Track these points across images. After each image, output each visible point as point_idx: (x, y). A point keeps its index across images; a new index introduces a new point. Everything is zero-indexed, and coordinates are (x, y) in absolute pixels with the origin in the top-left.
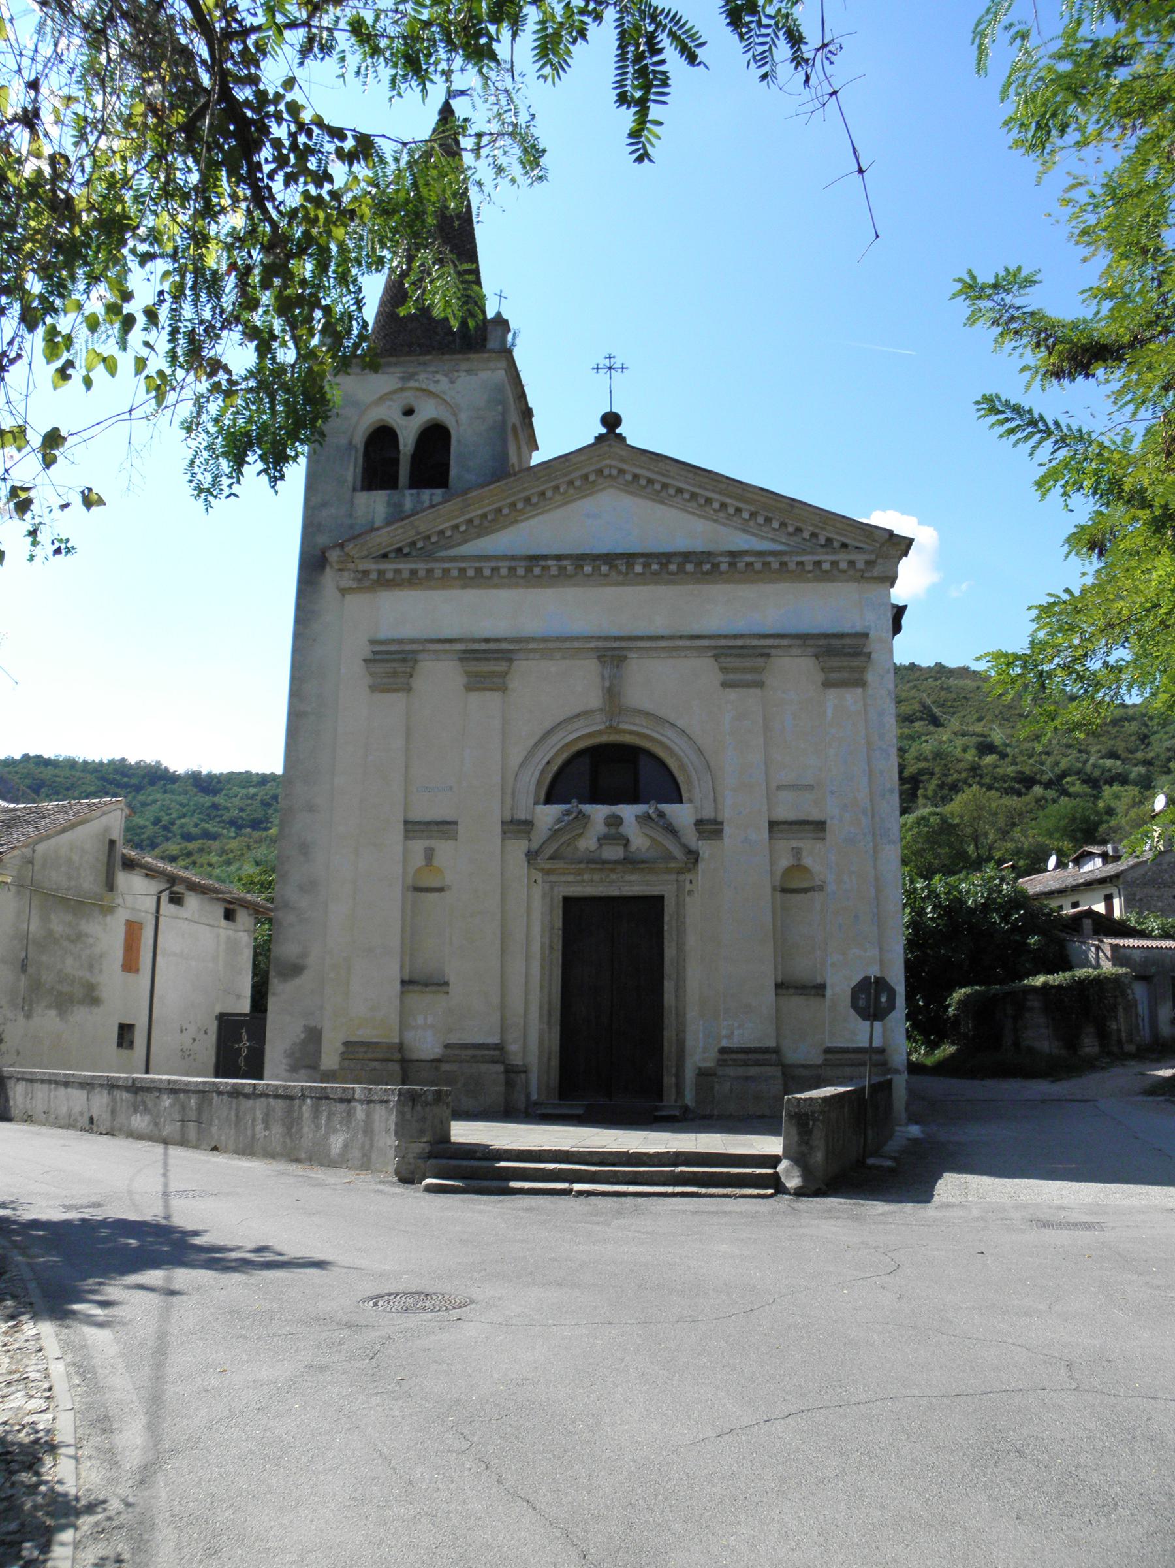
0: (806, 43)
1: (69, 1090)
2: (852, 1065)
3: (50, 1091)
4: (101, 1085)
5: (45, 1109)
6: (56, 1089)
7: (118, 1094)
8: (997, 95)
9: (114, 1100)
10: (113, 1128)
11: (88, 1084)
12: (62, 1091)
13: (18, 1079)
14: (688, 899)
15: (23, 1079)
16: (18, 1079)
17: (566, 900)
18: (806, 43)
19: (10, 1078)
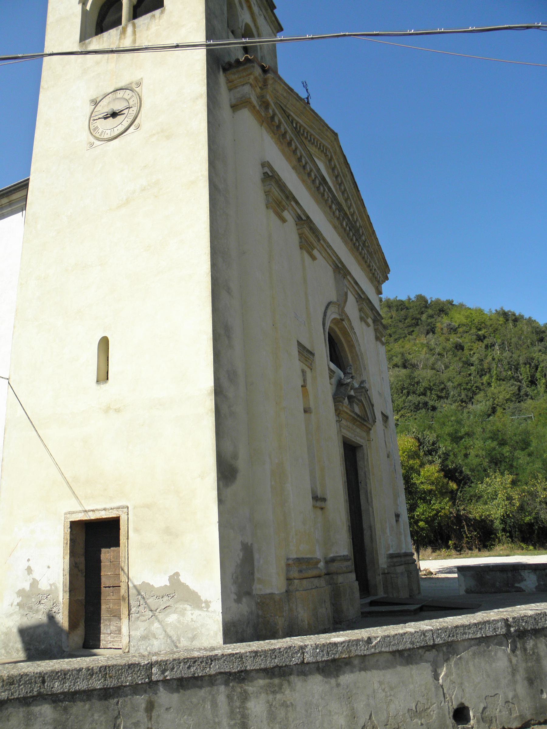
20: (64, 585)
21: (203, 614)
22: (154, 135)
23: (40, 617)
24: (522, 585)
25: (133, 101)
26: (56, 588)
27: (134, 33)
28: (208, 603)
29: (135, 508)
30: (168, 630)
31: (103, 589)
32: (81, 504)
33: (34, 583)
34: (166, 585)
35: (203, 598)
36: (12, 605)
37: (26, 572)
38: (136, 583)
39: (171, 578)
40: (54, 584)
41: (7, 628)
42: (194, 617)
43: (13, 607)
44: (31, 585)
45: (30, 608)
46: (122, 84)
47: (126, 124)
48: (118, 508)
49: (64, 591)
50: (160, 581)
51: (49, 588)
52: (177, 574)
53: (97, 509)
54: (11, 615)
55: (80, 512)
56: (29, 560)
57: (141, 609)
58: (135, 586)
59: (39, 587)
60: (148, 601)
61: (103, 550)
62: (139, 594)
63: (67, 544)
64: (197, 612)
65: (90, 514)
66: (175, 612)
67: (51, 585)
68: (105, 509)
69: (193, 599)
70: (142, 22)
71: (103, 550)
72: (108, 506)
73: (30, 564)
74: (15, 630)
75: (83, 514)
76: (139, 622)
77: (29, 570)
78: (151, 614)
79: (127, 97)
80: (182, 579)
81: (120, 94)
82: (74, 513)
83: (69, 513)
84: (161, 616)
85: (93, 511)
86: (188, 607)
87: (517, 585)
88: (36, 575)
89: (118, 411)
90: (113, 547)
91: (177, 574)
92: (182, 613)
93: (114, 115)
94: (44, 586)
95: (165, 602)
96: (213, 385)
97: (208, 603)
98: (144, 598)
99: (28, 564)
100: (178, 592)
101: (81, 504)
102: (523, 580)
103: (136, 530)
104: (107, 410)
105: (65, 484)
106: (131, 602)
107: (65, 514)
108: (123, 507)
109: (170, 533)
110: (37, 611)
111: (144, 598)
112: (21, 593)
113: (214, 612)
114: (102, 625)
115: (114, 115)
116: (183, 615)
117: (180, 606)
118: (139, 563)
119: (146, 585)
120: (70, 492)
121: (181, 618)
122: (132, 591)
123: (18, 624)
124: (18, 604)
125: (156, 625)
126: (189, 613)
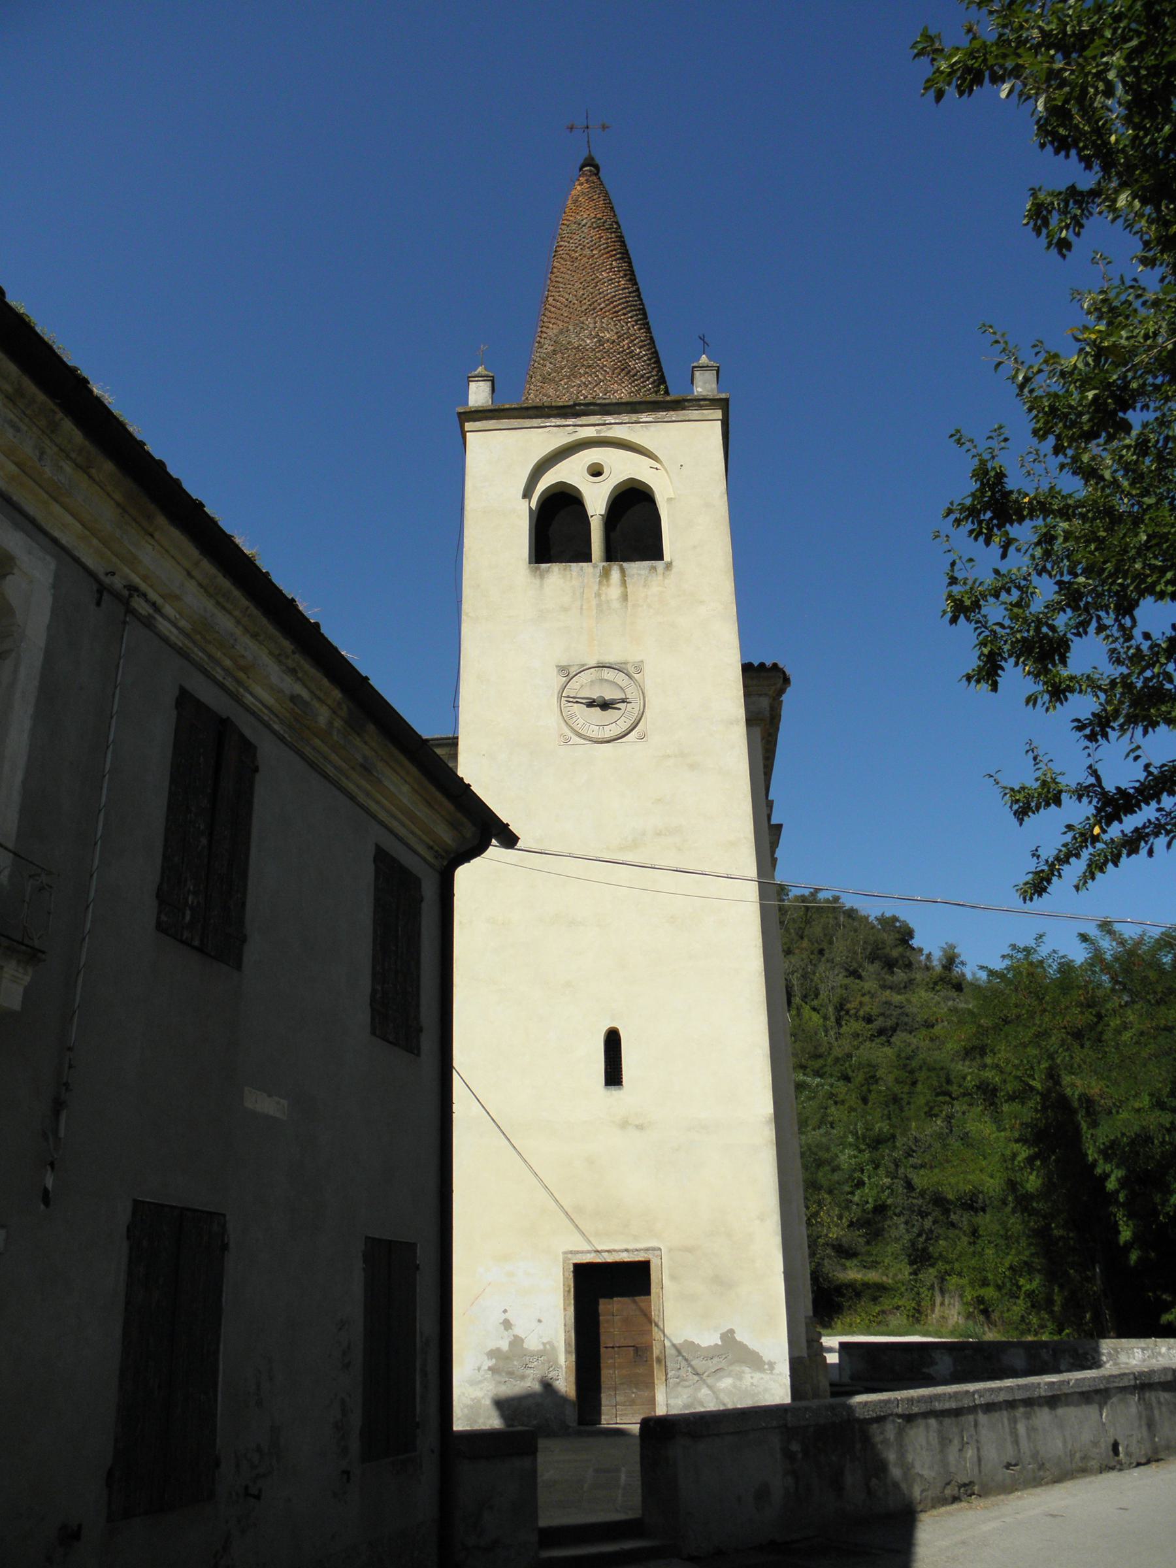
0: (1145, 732)
1: (1060, 1411)
2: (503, 410)
3: (1014, 1421)
4: (1123, 1389)
5: (1009, 1454)
6: (1028, 1417)
7: (1151, 1396)
8: (1061, 260)
9: (1149, 1407)
10: (1156, 1450)
11: (1097, 1392)
12: (1043, 1416)
13: (909, 1418)
14: (794, 893)
15: (926, 1415)
16: (909, 1418)
17: (415, 1245)
18: (1145, 732)
19: (880, 1419)
20: (567, 1344)
21: (766, 1377)
22: (669, 756)
23: (530, 1384)
24: (931, 1371)
25: (631, 693)
26: (554, 1348)
27: (624, 583)
28: (772, 1365)
29: (670, 1250)
30: (722, 1396)
31: (603, 1350)
32: (589, 1242)
33: (517, 1342)
34: (716, 1345)
35: (766, 1359)
36: (479, 1369)
37: (502, 1327)
38: (676, 1342)
39: (723, 1337)
40: (549, 1343)
41: (472, 1400)
42: (755, 1381)
43: (482, 1372)
44: (511, 1343)
45: (511, 1374)
46: (609, 659)
47: (623, 725)
48: (647, 1250)
49: (567, 1352)
50: (709, 1339)
51: (541, 1347)
52: (732, 1331)
53: (615, 1247)
54: (480, 1382)
55: (589, 1252)
56: (505, 1311)
57: (682, 1373)
58: (674, 1345)
59: (525, 1346)
60: (693, 1363)
61: (602, 1301)
62: (679, 1353)
63: (569, 1291)
64: (758, 1375)
65: (605, 1255)
66: (729, 1375)
67: (544, 1344)
68: (626, 1250)
69: (755, 1361)
70: (635, 571)
71: (602, 1301)
72: (630, 1247)
73: (507, 1316)
74: (488, 1402)
75: (593, 1255)
76: (680, 1389)
77: (507, 1324)
78: (696, 1378)
79: (623, 684)
80: (738, 1337)
81: (609, 675)
82: (578, 1252)
83: (571, 1252)
84: (710, 1381)
85: (608, 1251)
86: (747, 1370)
87: (925, 1370)
88: (518, 1331)
89: (640, 1127)
90: (617, 1296)
91: (732, 1331)
92: (739, 1376)
93: (605, 705)
94: (533, 1344)
95: (713, 1365)
96: (772, 1111)
97: (772, 1365)
98: (686, 1360)
99: (504, 1316)
100: (733, 1352)
101: (589, 1242)
102: (933, 1363)
103: (673, 1278)
104: (624, 1124)
105: (563, 1215)
106: (668, 1364)
107: (565, 1253)
108: (654, 1249)
109: (722, 1283)
110: (523, 1377)
111: (686, 1360)
112: (494, 1353)
113: (780, 1374)
114: (603, 1395)
115: (605, 705)
116: (740, 1379)
117: (737, 1368)
118: (681, 1316)
119: (691, 1345)
120: (572, 1227)
121: (738, 1383)
122: (670, 1351)
123: (491, 1394)
124: (490, 1369)
125: (705, 1391)
126: (748, 1376)
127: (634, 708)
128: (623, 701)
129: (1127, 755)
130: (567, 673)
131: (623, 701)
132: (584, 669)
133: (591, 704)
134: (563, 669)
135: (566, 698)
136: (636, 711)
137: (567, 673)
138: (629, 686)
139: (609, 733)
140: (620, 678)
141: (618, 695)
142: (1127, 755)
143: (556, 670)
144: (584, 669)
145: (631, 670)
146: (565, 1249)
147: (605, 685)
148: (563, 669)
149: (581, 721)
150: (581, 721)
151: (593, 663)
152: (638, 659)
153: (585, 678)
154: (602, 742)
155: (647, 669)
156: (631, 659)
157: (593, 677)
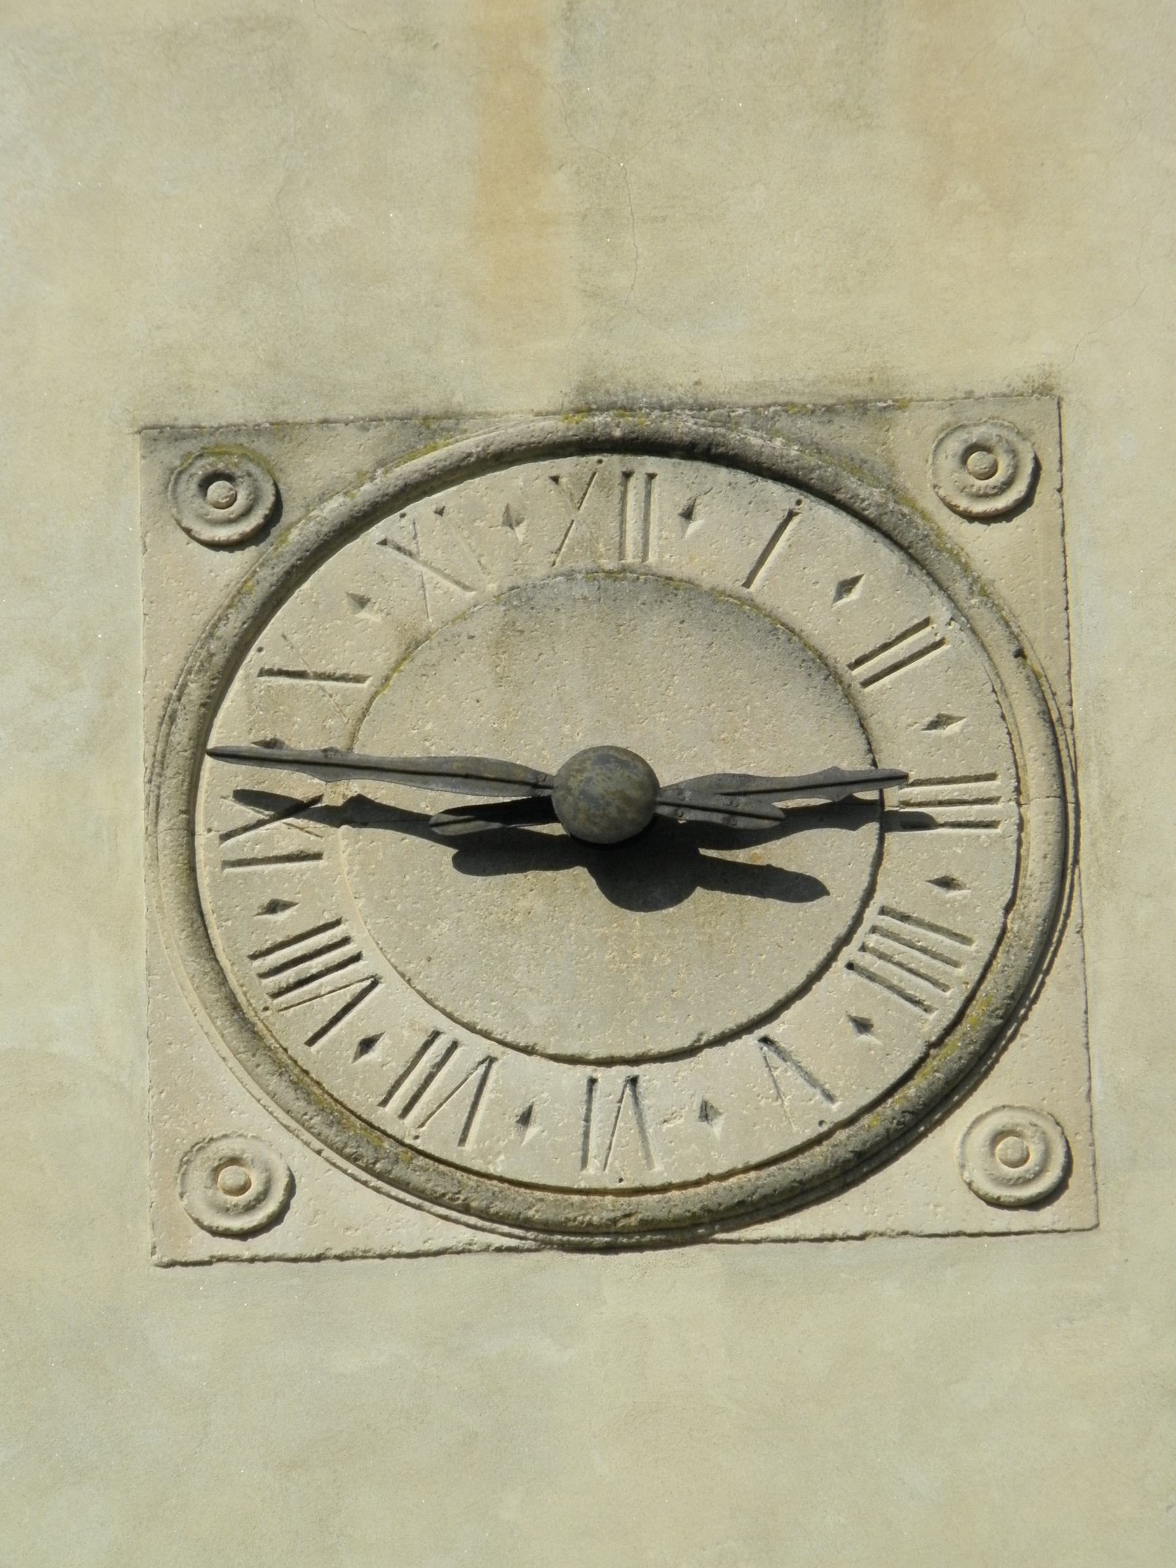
47: (838, 1061)
79: (842, 629)
81: (699, 527)
93: (655, 848)
115: (655, 848)
127: (950, 888)
128: (845, 804)
129: (291, 1189)
130: (256, 503)
131: (845, 804)
132: (438, 463)
133: (507, 829)
134: (215, 469)
135: (248, 773)
136: (978, 911)
137: (256, 503)
138: (897, 651)
139: (688, 1134)
140: (817, 568)
141: (794, 743)
142: (291, 1189)
143: (136, 476)
144: (438, 463)
145: (931, 479)
146: (361, 962)
147: (655, 626)
148: (215, 469)
149: (397, 1014)
150: (397, 1014)
151: (526, 403)
152: (1008, 363)
153: (442, 556)
154: (616, 1238)
155: (1101, 468)
156: (929, 364)
157: (534, 550)
